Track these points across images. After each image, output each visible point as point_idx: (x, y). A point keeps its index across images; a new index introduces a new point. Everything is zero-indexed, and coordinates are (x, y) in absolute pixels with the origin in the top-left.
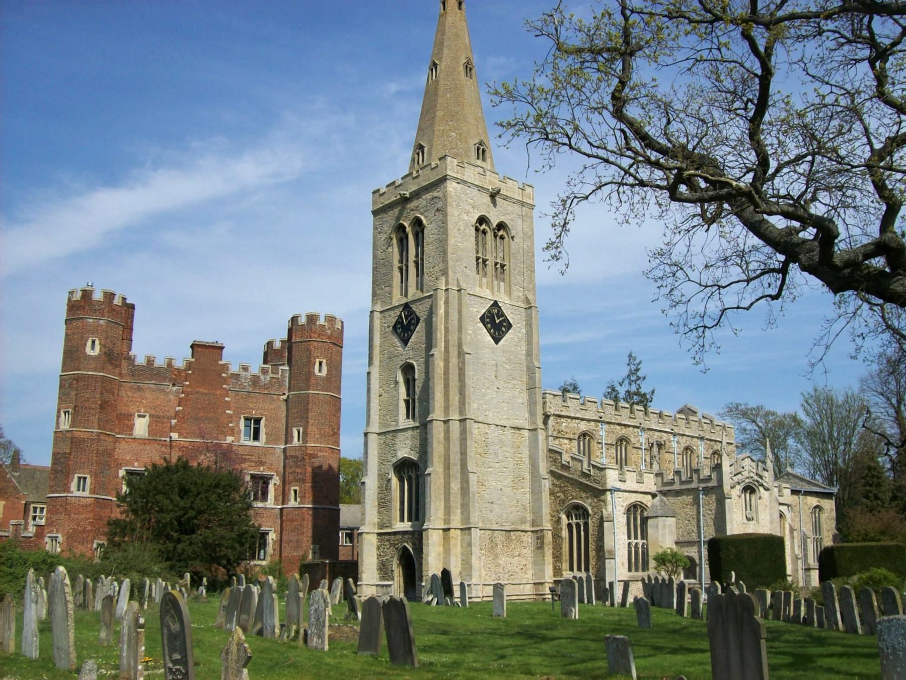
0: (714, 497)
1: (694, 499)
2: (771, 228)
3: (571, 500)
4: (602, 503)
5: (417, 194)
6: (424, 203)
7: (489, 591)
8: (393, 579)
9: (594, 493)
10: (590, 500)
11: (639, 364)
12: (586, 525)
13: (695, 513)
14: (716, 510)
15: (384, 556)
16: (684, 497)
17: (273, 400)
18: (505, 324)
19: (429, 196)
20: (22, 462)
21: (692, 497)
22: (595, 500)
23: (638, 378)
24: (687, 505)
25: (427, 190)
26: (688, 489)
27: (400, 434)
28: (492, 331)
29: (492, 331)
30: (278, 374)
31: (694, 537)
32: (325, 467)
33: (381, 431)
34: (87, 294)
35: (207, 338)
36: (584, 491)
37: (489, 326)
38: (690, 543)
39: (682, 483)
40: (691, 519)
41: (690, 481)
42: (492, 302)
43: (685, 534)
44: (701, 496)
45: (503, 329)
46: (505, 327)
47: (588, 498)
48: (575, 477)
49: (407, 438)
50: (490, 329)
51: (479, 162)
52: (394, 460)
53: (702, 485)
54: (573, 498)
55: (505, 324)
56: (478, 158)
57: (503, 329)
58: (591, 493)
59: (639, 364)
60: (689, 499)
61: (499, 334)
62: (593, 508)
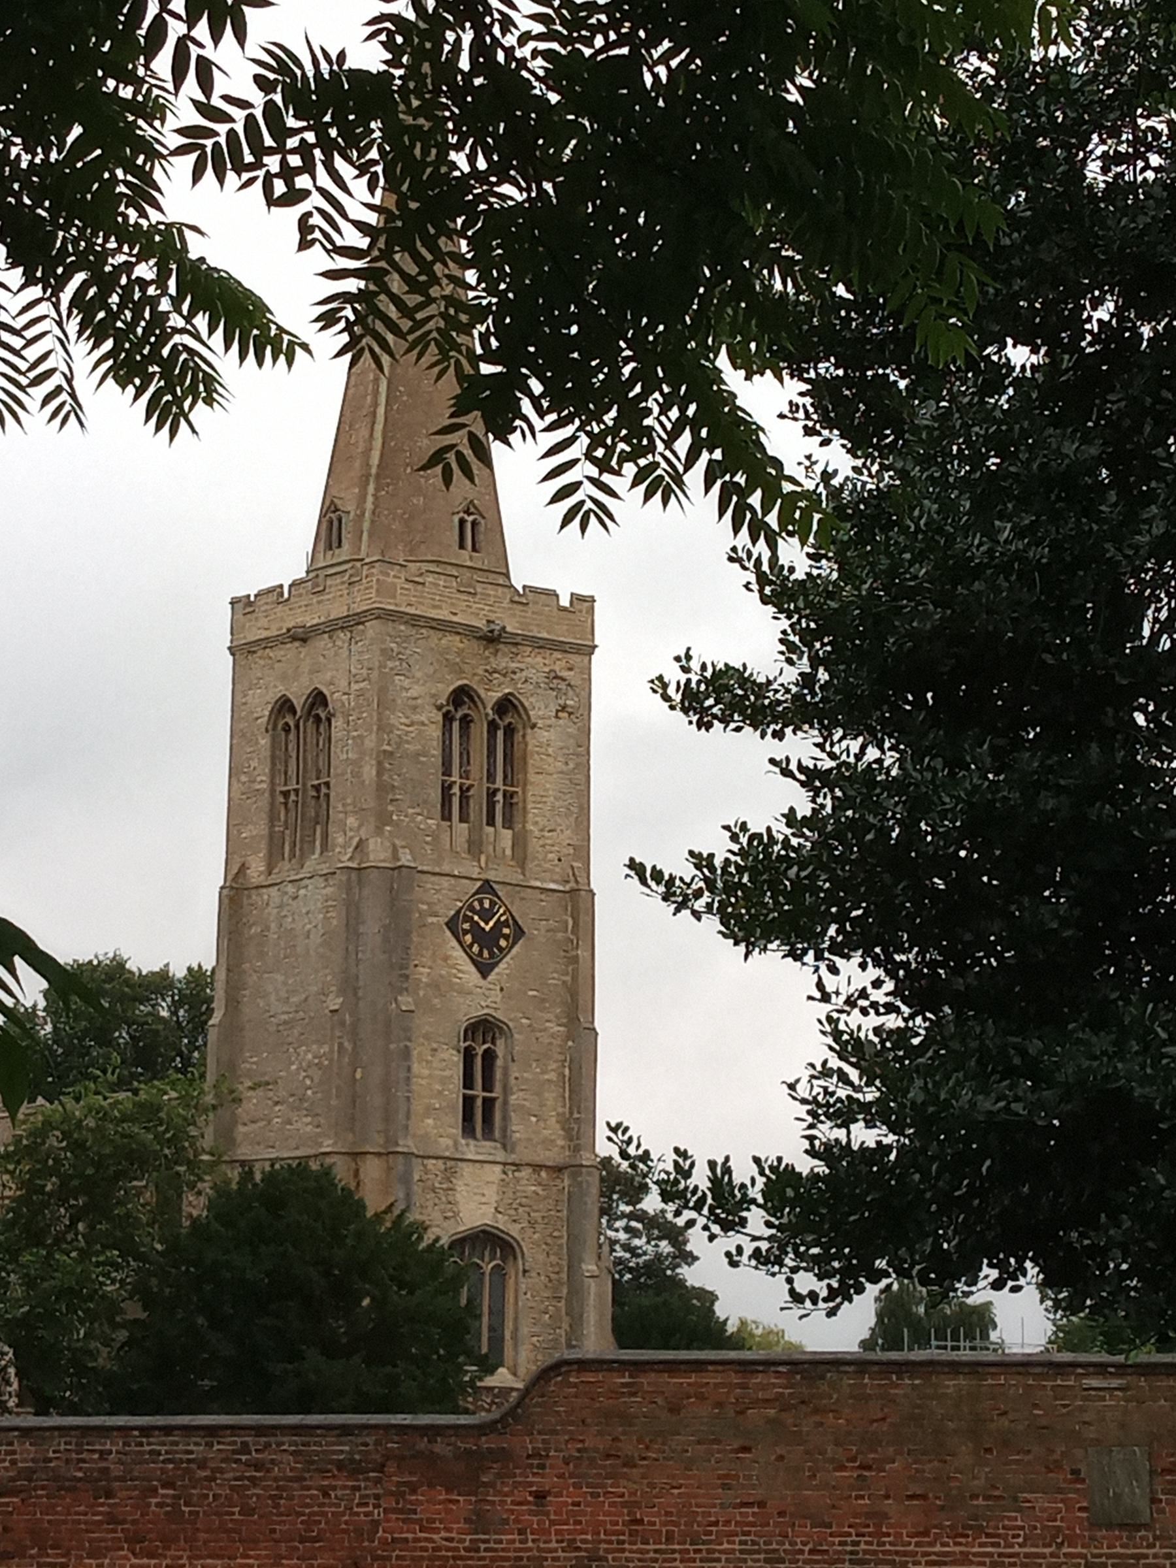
2: (127, 975)
7: (764, 680)
17: (44, 1439)
18: (506, 931)
20: (994, 1336)
28: (476, 948)
29: (476, 948)
30: (487, 923)
32: (721, 848)
34: (707, 730)
35: (860, 970)
37: (468, 938)
42: (479, 884)
45: (503, 943)
46: (506, 937)
50: (471, 946)
51: (465, 557)
55: (506, 931)
56: (462, 546)
57: (503, 943)
61: (492, 955)
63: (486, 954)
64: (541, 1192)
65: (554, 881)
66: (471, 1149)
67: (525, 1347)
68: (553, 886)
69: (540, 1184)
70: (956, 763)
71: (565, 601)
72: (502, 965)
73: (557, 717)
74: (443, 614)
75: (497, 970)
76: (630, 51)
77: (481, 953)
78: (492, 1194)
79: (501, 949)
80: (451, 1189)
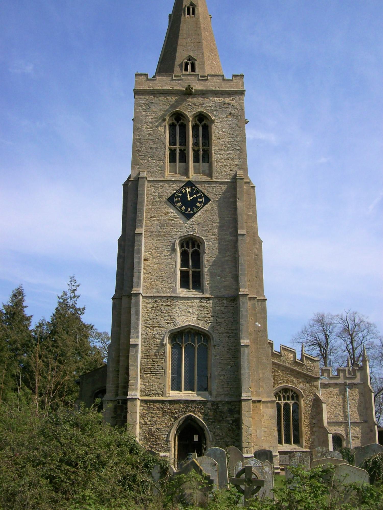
0: (357, 390)
1: (340, 392)
3: (281, 383)
4: (315, 388)
5: (203, 94)
6: (212, 104)
8: (169, 450)
9: (306, 379)
10: (301, 385)
11: (78, 286)
12: (297, 407)
13: (341, 401)
14: (359, 400)
15: (153, 426)
16: (331, 389)
19: (219, 100)
21: (338, 389)
22: (308, 385)
23: (75, 296)
24: (333, 395)
25: (216, 94)
26: (336, 384)
27: (179, 302)
31: (341, 419)
33: (148, 295)
36: (295, 377)
37: (179, 204)
38: (338, 424)
39: (346, 378)
40: (337, 405)
41: (338, 376)
43: (333, 416)
44: (347, 389)
45: (198, 205)
46: (200, 202)
47: (299, 383)
48: (287, 365)
49: (192, 308)
52: (171, 327)
53: (348, 382)
54: (283, 382)
57: (198, 205)
58: (303, 379)
59: (78, 286)
60: (336, 391)
62: (305, 391)
63: (189, 209)
64: (223, 310)
65: (227, 179)
66: (184, 293)
67: (216, 381)
68: (227, 181)
69: (223, 306)
70: (40, 335)
71: (276, 348)
72: (198, 214)
73: (227, 117)
74: (168, 88)
75: (195, 216)
76: (257, 322)
77: (186, 210)
78: (195, 312)
79: (197, 207)
80: (171, 310)
